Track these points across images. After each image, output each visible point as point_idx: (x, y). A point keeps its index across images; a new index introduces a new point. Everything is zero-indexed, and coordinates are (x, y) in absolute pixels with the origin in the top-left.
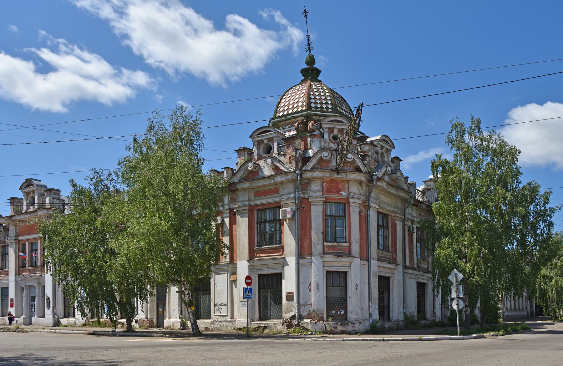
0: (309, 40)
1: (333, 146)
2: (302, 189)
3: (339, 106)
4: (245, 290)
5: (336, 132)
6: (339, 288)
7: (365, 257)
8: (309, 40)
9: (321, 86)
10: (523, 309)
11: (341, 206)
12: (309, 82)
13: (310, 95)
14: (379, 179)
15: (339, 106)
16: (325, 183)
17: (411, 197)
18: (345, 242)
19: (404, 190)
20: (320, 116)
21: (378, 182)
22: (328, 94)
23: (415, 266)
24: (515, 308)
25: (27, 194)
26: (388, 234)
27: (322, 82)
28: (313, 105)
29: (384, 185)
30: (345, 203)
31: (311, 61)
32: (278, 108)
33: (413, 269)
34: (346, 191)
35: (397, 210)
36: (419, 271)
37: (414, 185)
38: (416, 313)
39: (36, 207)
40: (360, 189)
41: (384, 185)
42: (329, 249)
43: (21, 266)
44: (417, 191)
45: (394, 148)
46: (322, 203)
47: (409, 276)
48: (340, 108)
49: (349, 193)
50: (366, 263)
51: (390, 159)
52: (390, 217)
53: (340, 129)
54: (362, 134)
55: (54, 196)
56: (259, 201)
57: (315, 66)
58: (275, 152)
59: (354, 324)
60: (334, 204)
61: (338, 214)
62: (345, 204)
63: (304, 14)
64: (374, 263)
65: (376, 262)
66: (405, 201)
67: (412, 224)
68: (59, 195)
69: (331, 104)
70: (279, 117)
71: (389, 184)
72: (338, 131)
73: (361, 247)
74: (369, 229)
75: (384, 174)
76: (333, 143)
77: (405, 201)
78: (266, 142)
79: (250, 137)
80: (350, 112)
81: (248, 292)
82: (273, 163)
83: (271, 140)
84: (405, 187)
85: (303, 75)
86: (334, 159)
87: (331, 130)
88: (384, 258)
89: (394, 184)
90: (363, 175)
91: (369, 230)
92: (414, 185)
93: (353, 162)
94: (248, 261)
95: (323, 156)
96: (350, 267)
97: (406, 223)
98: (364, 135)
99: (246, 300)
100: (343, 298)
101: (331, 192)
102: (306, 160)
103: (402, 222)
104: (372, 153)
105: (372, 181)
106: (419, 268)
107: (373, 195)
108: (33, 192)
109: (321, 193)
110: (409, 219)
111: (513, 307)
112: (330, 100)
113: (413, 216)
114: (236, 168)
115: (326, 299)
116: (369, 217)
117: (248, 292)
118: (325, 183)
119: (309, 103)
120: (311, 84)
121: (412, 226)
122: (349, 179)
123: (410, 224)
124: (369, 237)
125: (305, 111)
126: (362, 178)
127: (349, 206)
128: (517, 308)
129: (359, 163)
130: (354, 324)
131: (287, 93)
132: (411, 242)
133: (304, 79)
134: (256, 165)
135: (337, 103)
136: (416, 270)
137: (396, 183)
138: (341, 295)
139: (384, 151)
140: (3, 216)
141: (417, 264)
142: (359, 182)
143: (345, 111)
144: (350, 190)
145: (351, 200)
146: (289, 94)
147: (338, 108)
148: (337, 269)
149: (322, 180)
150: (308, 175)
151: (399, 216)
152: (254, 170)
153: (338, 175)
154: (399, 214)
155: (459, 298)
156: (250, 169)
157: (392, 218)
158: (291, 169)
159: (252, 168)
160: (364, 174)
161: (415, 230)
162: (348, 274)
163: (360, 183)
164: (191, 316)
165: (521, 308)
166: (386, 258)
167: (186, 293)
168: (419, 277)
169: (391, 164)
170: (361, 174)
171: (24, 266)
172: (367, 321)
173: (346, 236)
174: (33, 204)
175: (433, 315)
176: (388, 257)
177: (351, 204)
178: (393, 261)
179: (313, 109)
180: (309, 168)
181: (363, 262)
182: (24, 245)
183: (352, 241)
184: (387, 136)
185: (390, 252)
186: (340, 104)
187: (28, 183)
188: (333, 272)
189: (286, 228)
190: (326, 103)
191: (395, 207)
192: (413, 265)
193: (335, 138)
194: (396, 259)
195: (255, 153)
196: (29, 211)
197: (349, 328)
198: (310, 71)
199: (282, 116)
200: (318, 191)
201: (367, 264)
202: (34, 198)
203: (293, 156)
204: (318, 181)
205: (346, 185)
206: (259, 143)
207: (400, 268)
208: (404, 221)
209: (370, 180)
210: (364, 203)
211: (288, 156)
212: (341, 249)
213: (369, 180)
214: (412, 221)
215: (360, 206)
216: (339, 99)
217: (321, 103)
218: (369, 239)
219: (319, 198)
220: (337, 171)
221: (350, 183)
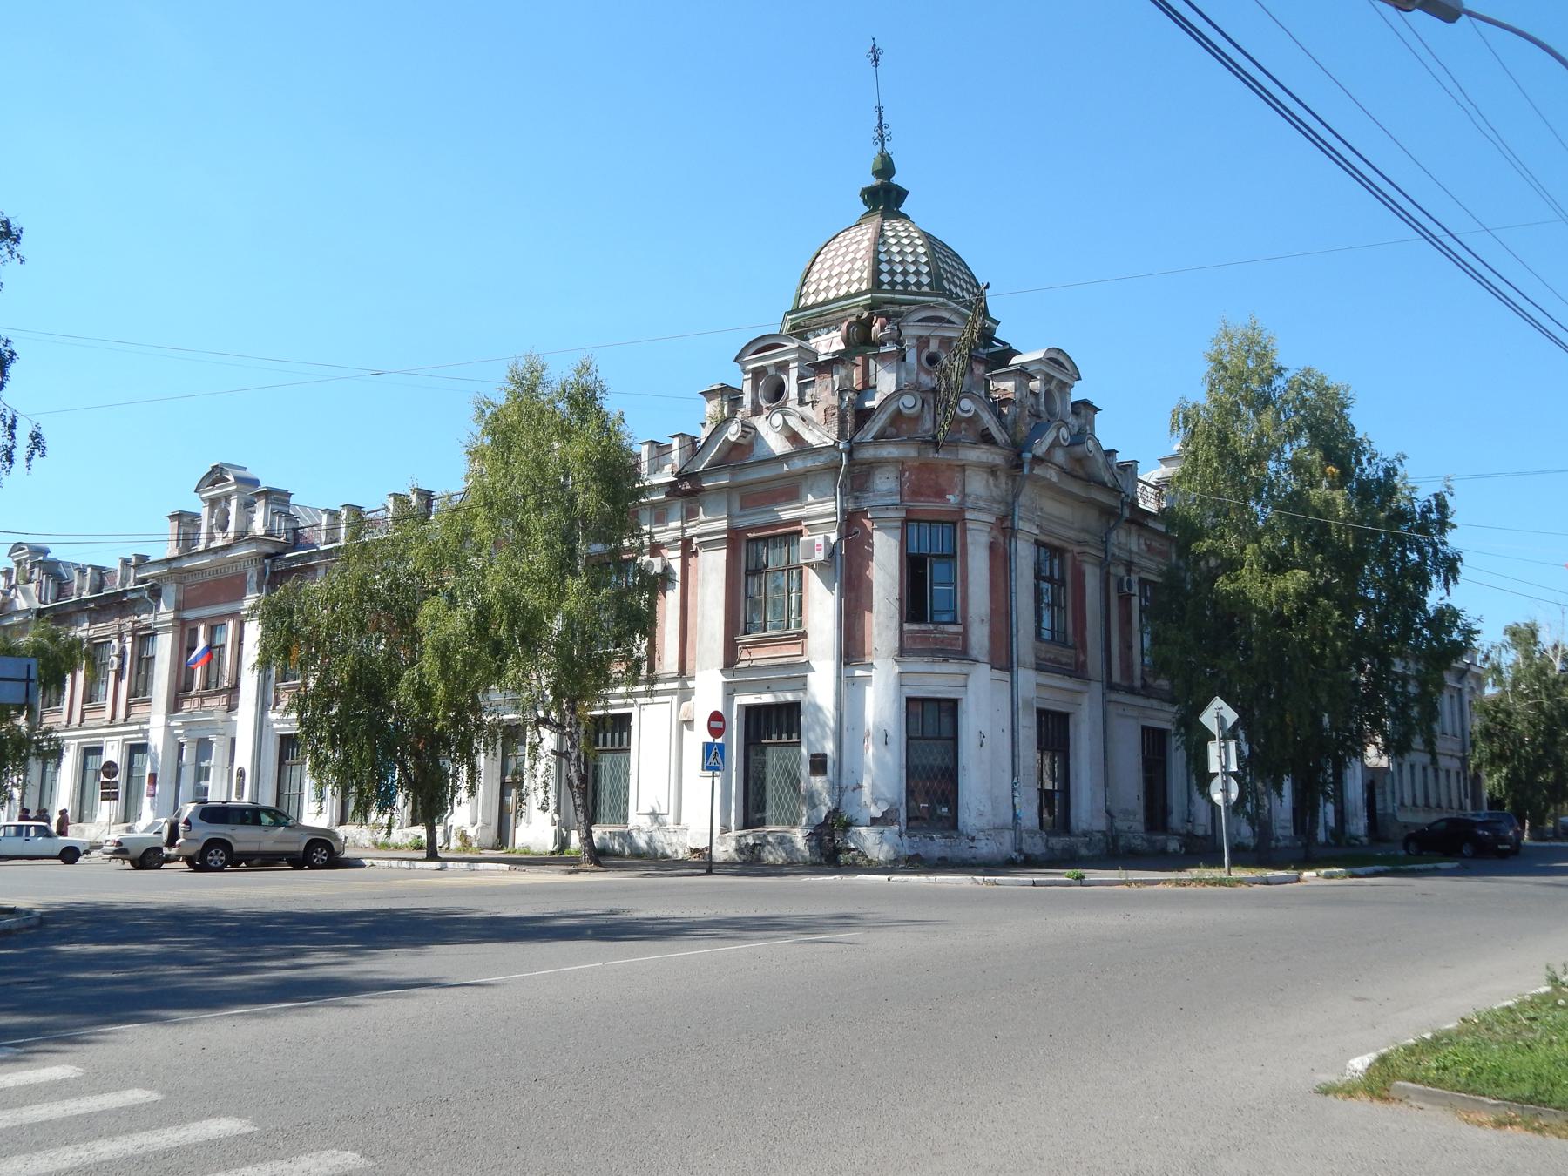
0: (881, 118)
1: (927, 380)
2: (852, 488)
3: (947, 279)
4: (708, 748)
5: (934, 346)
6: (940, 742)
7: (1003, 659)
8: (881, 118)
9: (906, 230)
10: (1414, 804)
11: (946, 530)
12: (878, 219)
13: (880, 252)
14: (1037, 460)
15: (947, 279)
16: (907, 473)
17: (1122, 501)
18: (955, 622)
19: (1103, 484)
20: (901, 303)
21: (1036, 467)
22: (919, 242)
23: (1138, 683)
24: (1427, 805)
25: (213, 502)
26: (1065, 598)
27: (908, 218)
28: (885, 278)
29: (1052, 475)
30: (954, 523)
31: (885, 168)
32: (804, 284)
33: (1131, 691)
34: (957, 492)
35: (1088, 537)
36: (1148, 696)
37: (1129, 469)
38: (1140, 816)
39: (232, 535)
40: (992, 485)
41: (1052, 475)
42: (914, 639)
43: (181, 690)
44: (1140, 485)
45: (1080, 379)
46: (899, 524)
47: (1120, 711)
48: (949, 282)
49: (964, 495)
50: (1006, 676)
51: (1069, 408)
52: (1068, 556)
53: (943, 337)
54: (1004, 344)
55: (276, 507)
56: (754, 517)
57: (895, 180)
58: (791, 397)
59: (973, 839)
60: (928, 524)
61: (938, 550)
62: (954, 523)
63: (872, 57)
64: (1028, 679)
65: (1032, 673)
66: (1107, 512)
67: (1129, 572)
68: (287, 503)
69: (928, 274)
70: (806, 308)
71: (1062, 470)
72: (940, 342)
73: (993, 635)
74: (1014, 588)
75: (1052, 446)
76: (928, 373)
77: (1107, 512)
78: (772, 371)
79: (735, 361)
80: (975, 291)
81: (713, 753)
82: (785, 422)
83: (783, 367)
84: (1107, 478)
85: (865, 203)
86: (929, 413)
87: (923, 342)
88: (1053, 662)
89: (1080, 472)
90: (998, 451)
91: (1014, 591)
92: (1129, 469)
93: (973, 420)
94: (721, 670)
95: (901, 407)
96: (965, 686)
97: (1113, 570)
98: (1007, 347)
99: (710, 773)
100: (947, 768)
101: (922, 495)
102: (863, 416)
103: (1101, 569)
104: (1022, 394)
105: (1020, 466)
106: (1147, 691)
107: (1022, 499)
108: (227, 498)
109: (896, 500)
110: (1119, 559)
111: (1420, 801)
112: (925, 263)
113: (1131, 552)
114: (703, 435)
115: (905, 771)
116: (1013, 557)
117: (713, 753)
118: (907, 473)
119: (876, 272)
120: (882, 226)
121: (1127, 578)
122: (963, 462)
123: (1121, 571)
124: (1014, 608)
125: (865, 293)
126: (994, 456)
127: (964, 531)
128: (1433, 802)
129: (989, 421)
130: (973, 839)
131: (826, 249)
132: (1126, 621)
133: (867, 213)
134: (748, 430)
135: (942, 271)
136: (1138, 694)
137: (1083, 467)
138: (943, 760)
139: (1053, 386)
140: (151, 559)
141: (1142, 678)
142: (988, 467)
143: (962, 289)
144: (967, 491)
145: (968, 515)
146: (829, 251)
147: (945, 283)
148: (934, 692)
149: (901, 463)
150: (868, 453)
151: (1093, 552)
152: (742, 441)
153: (937, 451)
154: (1091, 546)
155: (1226, 773)
156: (733, 439)
157: (1074, 558)
158: (827, 440)
159: (737, 436)
160: (1002, 448)
161: (1135, 589)
162: (962, 707)
163: (993, 471)
164: (581, 817)
165: (1444, 804)
166: (1060, 663)
167: (574, 756)
168: (1149, 712)
169: (1071, 419)
170: (994, 449)
171: (189, 686)
172: (1007, 832)
173: (955, 606)
174: (224, 528)
175: (1186, 818)
176: (1064, 660)
177: (970, 525)
178: (1077, 671)
179: (886, 287)
180: (869, 438)
181: (998, 674)
182: (195, 632)
183: (970, 619)
184: (1060, 351)
185: (1070, 648)
186: (950, 272)
187: (216, 476)
188: (923, 700)
189: (813, 581)
190: (917, 273)
191: (1083, 530)
192: (1133, 681)
193: (933, 360)
194: (1084, 664)
195: (747, 398)
196: (213, 545)
197: (962, 850)
198: (881, 193)
199: (813, 306)
200: (890, 493)
201: (1009, 680)
202: (228, 514)
203: (834, 407)
204: (891, 468)
205: (958, 477)
206: (757, 374)
207: (1096, 688)
208: (1104, 564)
209: (1016, 464)
210: (1002, 522)
211: (821, 406)
212: (942, 642)
213: (1014, 463)
214: (1129, 566)
215: (991, 528)
216: (948, 260)
217: (905, 273)
218: (1014, 613)
219: (891, 509)
220: (935, 444)
221: (967, 473)
